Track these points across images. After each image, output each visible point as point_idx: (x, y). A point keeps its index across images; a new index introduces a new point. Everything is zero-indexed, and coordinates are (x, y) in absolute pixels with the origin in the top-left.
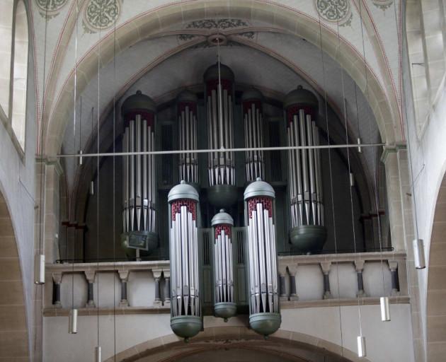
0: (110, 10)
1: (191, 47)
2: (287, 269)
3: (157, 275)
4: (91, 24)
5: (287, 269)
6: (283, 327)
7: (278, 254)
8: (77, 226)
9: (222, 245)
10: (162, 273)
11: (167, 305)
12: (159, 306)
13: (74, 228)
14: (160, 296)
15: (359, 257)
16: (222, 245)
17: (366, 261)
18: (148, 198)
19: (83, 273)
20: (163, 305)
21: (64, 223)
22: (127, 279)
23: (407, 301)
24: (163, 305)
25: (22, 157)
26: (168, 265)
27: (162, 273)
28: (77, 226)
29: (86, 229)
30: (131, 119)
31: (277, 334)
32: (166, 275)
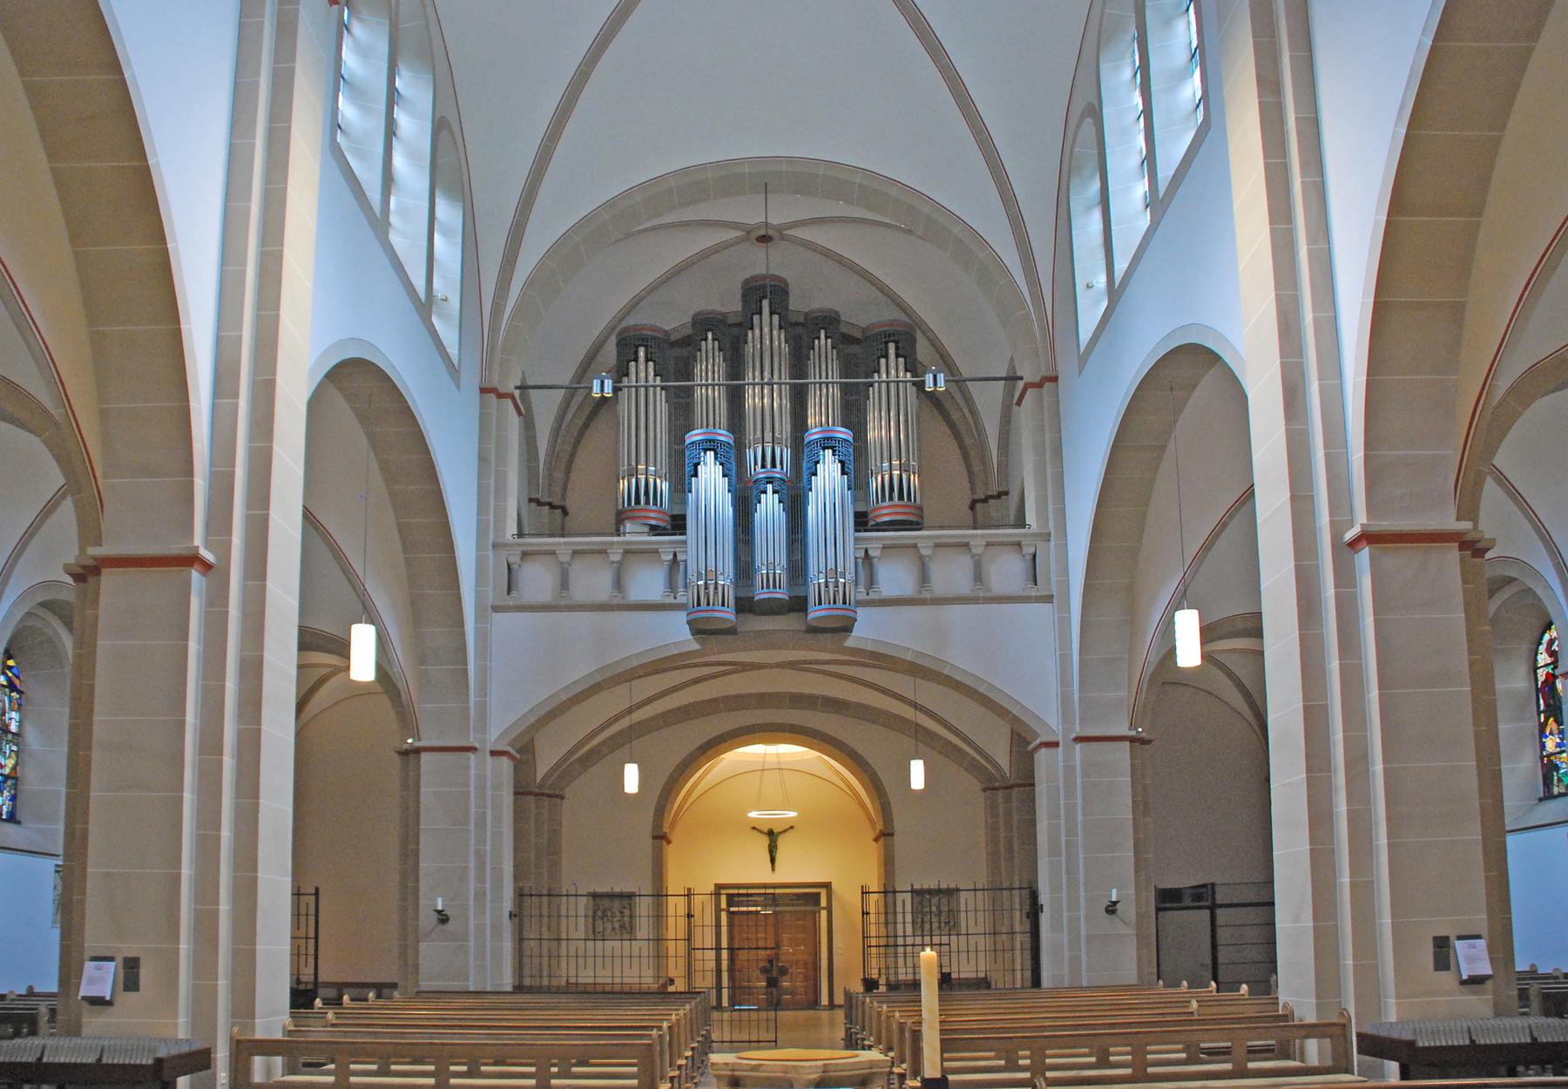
22: (620, 563)
23: (1049, 599)
24: (675, 598)
25: (454, 371)
27: (675, 555)
32: (679, 557)
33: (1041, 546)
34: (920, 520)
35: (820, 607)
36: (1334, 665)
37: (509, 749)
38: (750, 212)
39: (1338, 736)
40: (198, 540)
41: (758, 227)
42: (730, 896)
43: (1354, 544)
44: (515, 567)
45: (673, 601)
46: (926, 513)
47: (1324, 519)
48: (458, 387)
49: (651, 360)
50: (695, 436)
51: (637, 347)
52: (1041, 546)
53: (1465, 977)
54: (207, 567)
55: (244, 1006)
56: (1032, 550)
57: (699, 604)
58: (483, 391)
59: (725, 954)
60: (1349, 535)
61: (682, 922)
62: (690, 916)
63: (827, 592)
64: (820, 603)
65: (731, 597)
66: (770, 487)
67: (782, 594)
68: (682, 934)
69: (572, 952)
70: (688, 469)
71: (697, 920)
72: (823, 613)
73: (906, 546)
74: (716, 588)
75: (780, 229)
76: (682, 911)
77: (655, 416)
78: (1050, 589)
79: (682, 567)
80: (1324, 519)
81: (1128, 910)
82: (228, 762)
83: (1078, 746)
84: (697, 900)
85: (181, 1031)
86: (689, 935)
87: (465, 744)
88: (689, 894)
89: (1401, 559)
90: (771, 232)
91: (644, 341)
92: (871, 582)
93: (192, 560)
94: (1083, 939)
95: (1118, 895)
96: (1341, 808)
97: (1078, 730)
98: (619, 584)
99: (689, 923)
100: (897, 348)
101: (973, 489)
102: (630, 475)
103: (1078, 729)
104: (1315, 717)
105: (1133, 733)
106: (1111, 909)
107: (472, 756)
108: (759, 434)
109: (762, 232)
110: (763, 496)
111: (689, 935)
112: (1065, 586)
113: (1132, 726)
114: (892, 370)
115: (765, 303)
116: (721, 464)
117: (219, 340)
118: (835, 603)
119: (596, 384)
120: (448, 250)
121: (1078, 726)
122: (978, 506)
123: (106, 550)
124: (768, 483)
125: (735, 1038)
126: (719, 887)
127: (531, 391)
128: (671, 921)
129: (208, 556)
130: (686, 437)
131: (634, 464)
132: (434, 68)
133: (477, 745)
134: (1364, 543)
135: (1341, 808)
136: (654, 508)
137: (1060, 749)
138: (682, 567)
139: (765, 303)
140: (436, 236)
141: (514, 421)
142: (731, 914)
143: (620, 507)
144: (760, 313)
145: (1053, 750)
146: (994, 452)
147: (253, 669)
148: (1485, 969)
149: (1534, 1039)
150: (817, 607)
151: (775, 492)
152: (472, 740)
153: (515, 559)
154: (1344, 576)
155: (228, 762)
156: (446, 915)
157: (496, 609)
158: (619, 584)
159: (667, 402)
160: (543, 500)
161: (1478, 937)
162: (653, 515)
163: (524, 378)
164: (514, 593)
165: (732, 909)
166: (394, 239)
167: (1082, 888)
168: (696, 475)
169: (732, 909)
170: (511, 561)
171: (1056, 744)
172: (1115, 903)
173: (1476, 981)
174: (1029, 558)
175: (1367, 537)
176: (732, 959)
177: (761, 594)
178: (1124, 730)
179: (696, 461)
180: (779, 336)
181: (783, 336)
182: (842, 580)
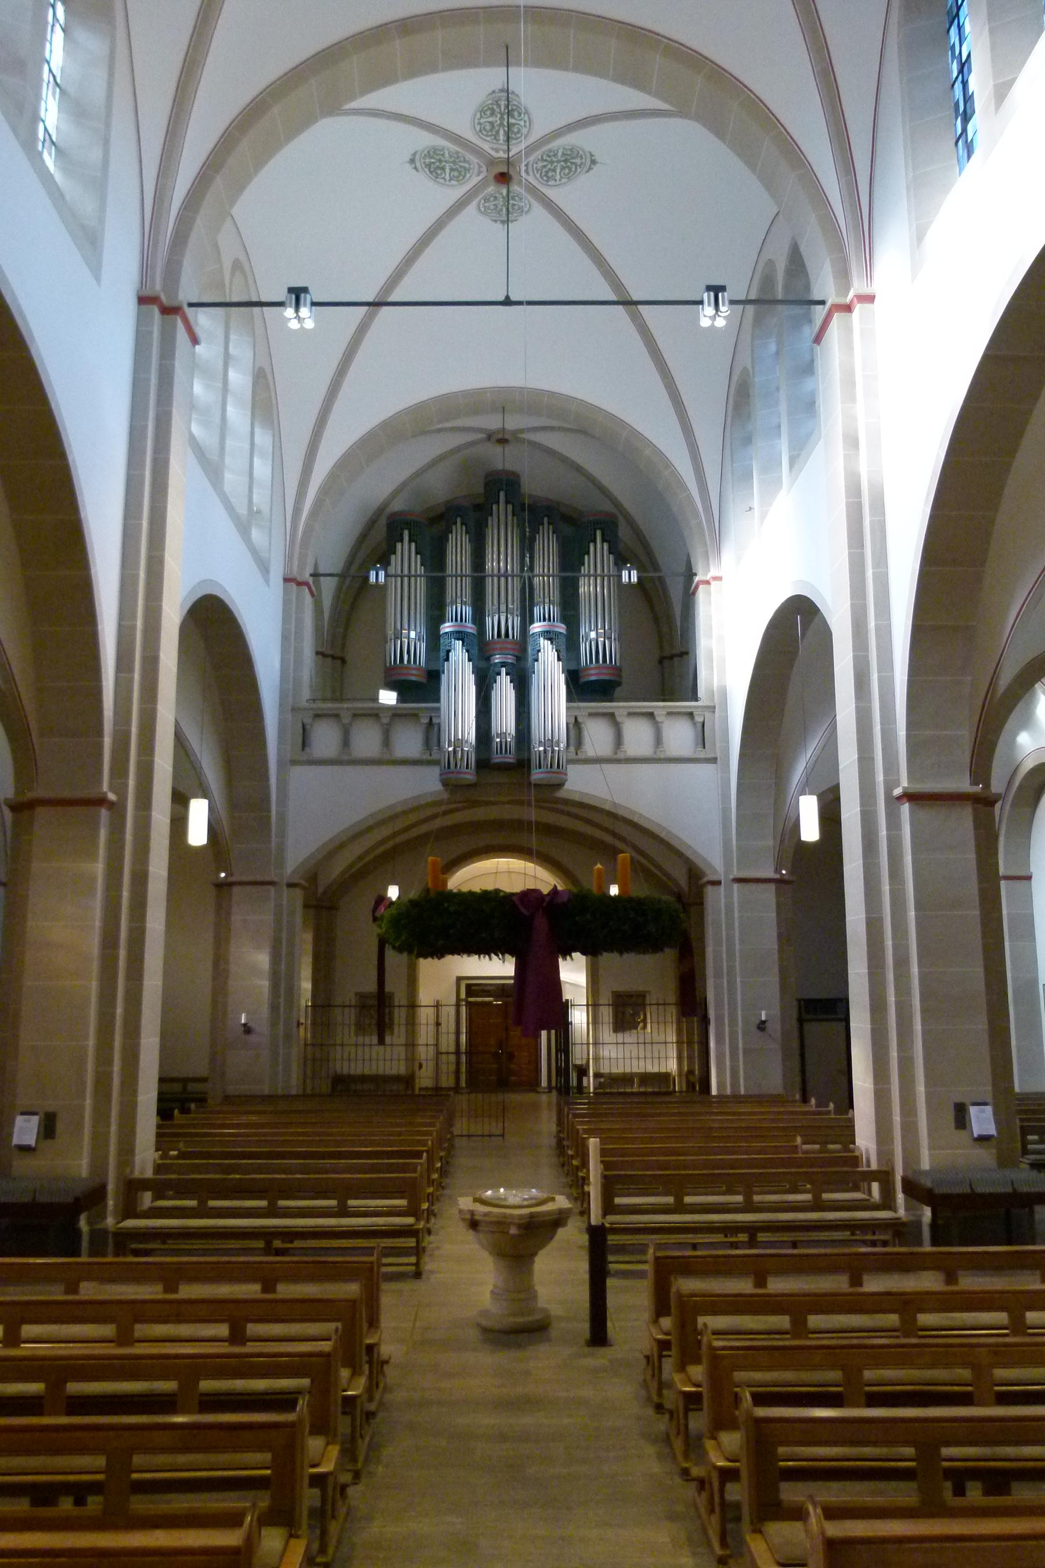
0: (457, 170)
1: (355, 600)
2: (576, 718)
3: (426, 721)
4: (422, 161)
5: (576, 718)
6: (568, 786)
7: (570, 699)
8: (333, 657)
9: (504, 692)
10: (431, 719)
11: (435, 756)
12: (426, 757)
13: (330, 659)
14: (427, 743)
15: (659, 707)
16: (504, 692)
17: (355, 715)
18: (415, 630)
19: (691, 715)
20: (431, 755)
21: (317, 653)
22: (389, 724)
23: (714, 760)
24: (431, 755)
25: (264, 569)
26: (438, 709)
27: (431, 719)
28: (333, 657)
29: (343, 661)
30: (398, 541)
31: (561, 794)
32: (435, 721)
33: (708, 715)
34: (617, 679)
35: (540, 770)
36: (886, 888)
37: (302, 882)
38: (493, 422)
39: (889, 943)
40: (105, 787)
41: (498, 431)
42: (468, 986)
43: (899, 798)
44: (308, 727)
45: (429, 758)
46: (624, 674)
47: (880, 777)
48: (268, 586)
49: (413, 541)
50: (447, 627)
51: (402, 530)
52: (708, 715)
53: (975, 1135)
54: (111, 805)
55: (127, 1149)
56: (701, 720)
57: (449, 767)
58: (286, 580)
59: (463, 1058)
60: (898, 791)
61: (432, 1028)
62: (438, 1024)
63: (546, 757)
64: (540, 768)
65: (473, 759)
66: (503, 670)
67: (510, 759)
68: (431, 1041)
69: (346, 1056)
70: (443, 654)
71: (443, 1028)
72: (542, 776)
73: (604, 715)
74: (462, 753)
75: (515, 432)
76: (432, 1019)
77: (416, 598)
78: (715, 753)
79: (436, 728)
80: (880, 777)
81: (775, 1028)
82: (122, 953)
83: (736, 886)
84: (444, 1011)
85: (81, 1166)
86: (437, 1040)
87: (267, 879)
88: (437, 1006)
89: (930, 815)
90: (507, 436)
91: (408, 524)
92: (579, 743)
93: (101, 801)
94: (741, 1052)
95: (767, 1015)
96: (891, 999)
97: (736, 873)
98: (386, 742)
99: (437, 1031)
100: (603, 535)
101: (661, 648)
102: (396, 638)
103: (735, 873)
104: (873, 925)
105: (778, 876)
106: (762, 1026)
107: (272, 889)
108: (496, 607)
109: (500, 436)
110: (498, 678)
111: (437, 1040)
112: (726, 749)
113: (777, 870)
114: (598, 553)
115: (502, 494)
116: (467, 651)
117: (120, 627)
118: (551, 767)
119: (373, 574)
120: (262, 469)
121: (735, 869)
122: (666, 663)
123: (40, 792)
124: (502, 666)
125: (473, 1131)
126: (459, 979)
127: (322, 578)
128: (423, 1028)
129: (112, 797)
130: (442, 627)
131: (399, 628)
132: (254, 333)
133: (276, 879)
134: (905, 800)
135: (891, 999)
136: (414, 666)
137: (722, 888)
138: (436, 728)
139: (502, 494)
140: (255, 459)
141: (308, 599)
142: (469, 1005)
143: (388, 665)
144: (498, 503)
145: (716, 888)
146: (679, 624)
147: (141, 879)
148: (991, 1130)
149: (1014, 1190)
150: (539, 770)
151: (507, 674)
152: (272, 877)
153: (307, 721)
154: (893, 823)
155: (122, 953)
156: (249, 1027)
157: (294, 762)
158: (386, 742)
159: (422, 565)
160: (327, 653)
161: (985, 1104)
162: (414, 672)
163: (316, 566)
164: (307, 749)
165: (470, 999)
166: (227, 488)
167: (727, 1026)
168: (447, 659)
169: (470, 999)
170: (305, 721)
171: (719, 883)
172: (764, 1022)
173: (983, 1139)
174: (699, 725)
175: (910, 797)
176: (469, 1063)
177: (497, 758)
178: (770, 874)
179: (448, 648)
180: (513, 520)
181: (515, 521)
182: (557, 749)
